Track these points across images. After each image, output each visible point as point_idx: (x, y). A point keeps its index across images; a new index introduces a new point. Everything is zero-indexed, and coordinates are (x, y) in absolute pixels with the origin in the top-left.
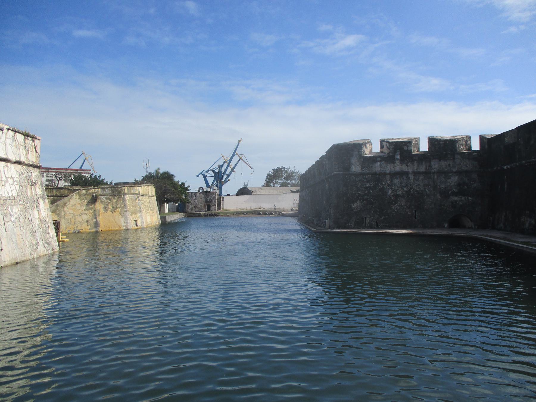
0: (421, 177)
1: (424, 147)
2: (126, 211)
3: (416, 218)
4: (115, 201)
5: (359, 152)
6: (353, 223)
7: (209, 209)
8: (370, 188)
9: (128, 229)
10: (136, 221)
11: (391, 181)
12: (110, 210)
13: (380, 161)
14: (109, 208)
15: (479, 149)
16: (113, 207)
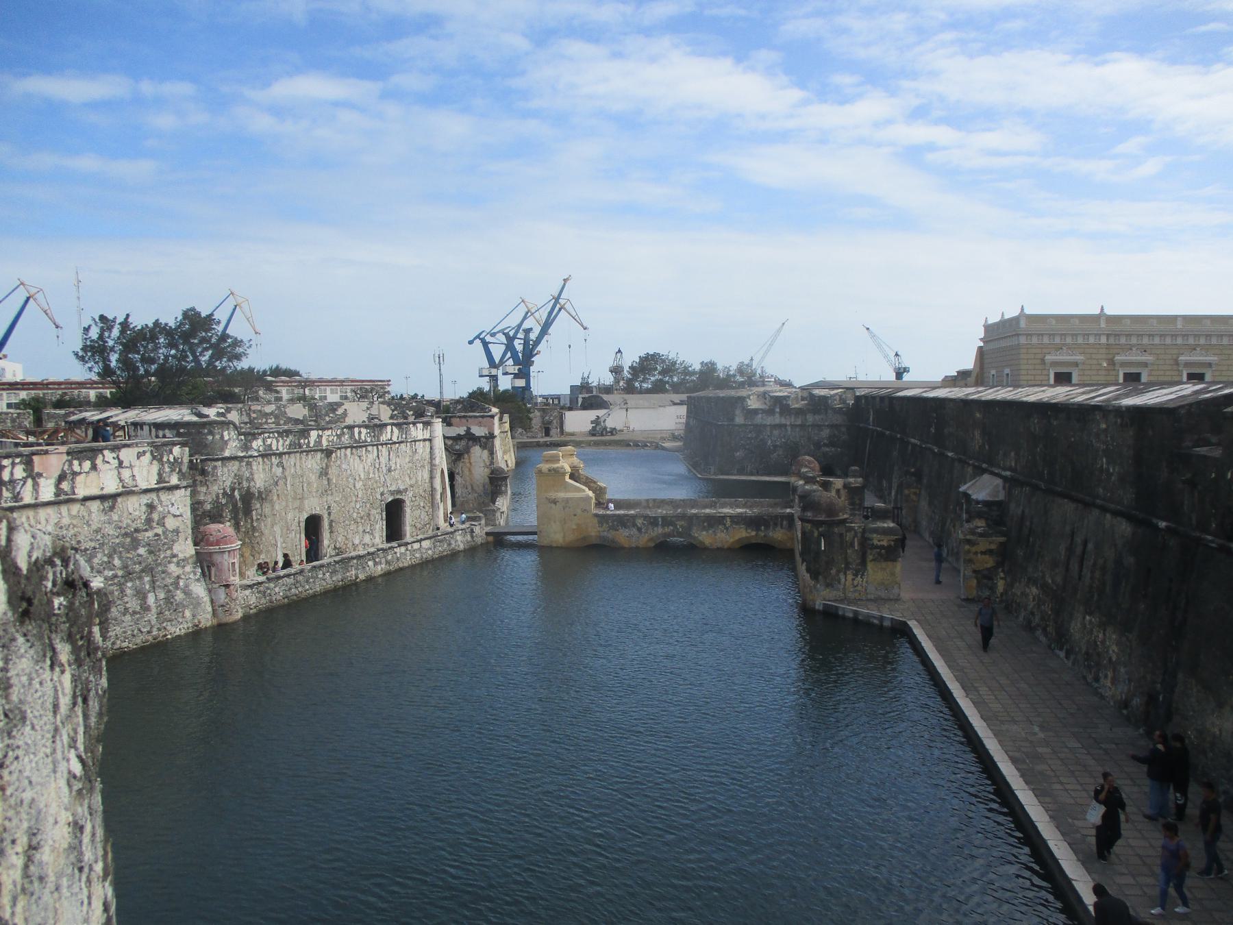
7: (547, 434)
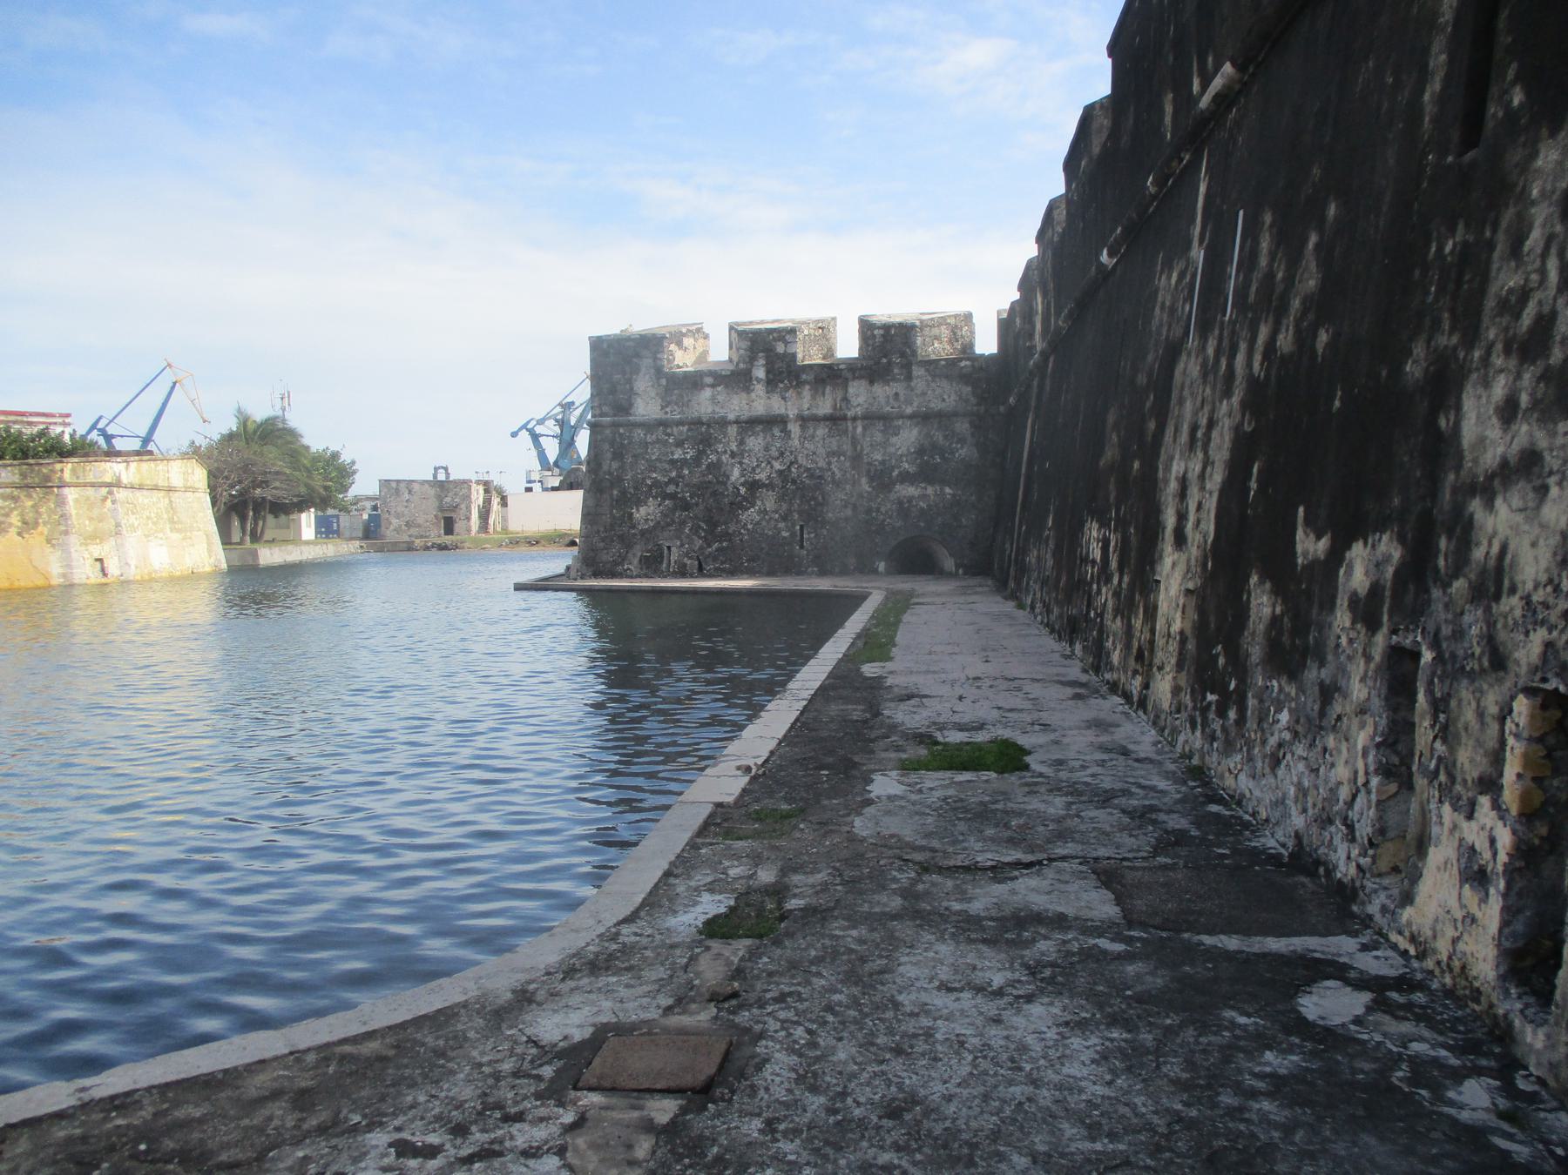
0: (821, 431)
1: (848, 347)
2: (66, 533)
3: (802, 547)
4: (30, 503)
5: (655, 359)
6: (636, 561)
8: (684, 462)
9: (72, 585)
10: (100, 560)
11: (742, 443)
12: (13, 531)
13: (713, 386)
14: (11, 525)
15: (854, 353)
16: (25, 523)
